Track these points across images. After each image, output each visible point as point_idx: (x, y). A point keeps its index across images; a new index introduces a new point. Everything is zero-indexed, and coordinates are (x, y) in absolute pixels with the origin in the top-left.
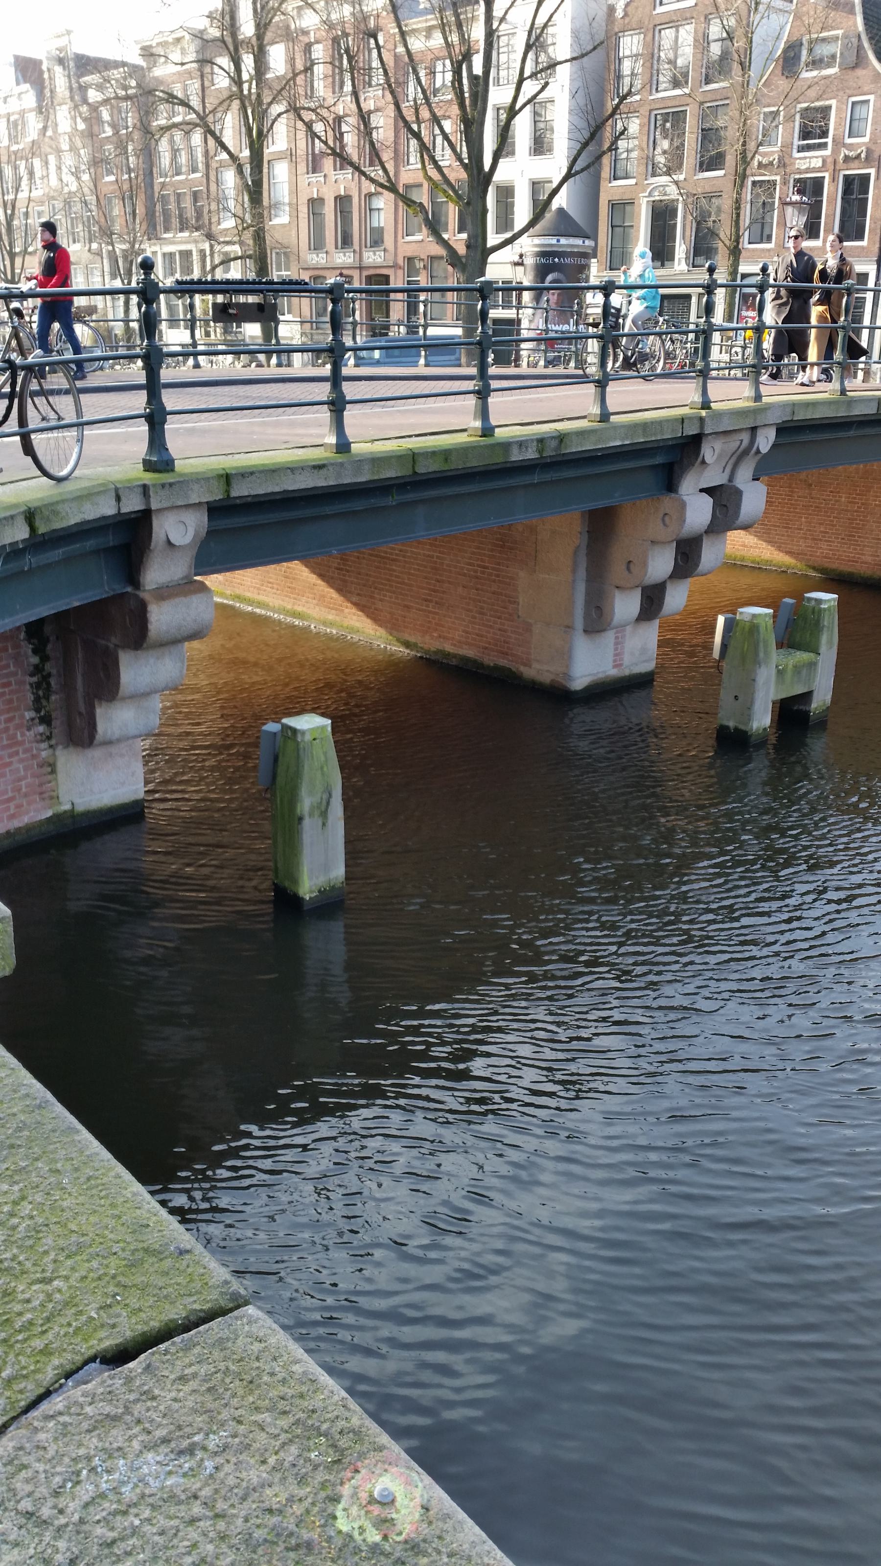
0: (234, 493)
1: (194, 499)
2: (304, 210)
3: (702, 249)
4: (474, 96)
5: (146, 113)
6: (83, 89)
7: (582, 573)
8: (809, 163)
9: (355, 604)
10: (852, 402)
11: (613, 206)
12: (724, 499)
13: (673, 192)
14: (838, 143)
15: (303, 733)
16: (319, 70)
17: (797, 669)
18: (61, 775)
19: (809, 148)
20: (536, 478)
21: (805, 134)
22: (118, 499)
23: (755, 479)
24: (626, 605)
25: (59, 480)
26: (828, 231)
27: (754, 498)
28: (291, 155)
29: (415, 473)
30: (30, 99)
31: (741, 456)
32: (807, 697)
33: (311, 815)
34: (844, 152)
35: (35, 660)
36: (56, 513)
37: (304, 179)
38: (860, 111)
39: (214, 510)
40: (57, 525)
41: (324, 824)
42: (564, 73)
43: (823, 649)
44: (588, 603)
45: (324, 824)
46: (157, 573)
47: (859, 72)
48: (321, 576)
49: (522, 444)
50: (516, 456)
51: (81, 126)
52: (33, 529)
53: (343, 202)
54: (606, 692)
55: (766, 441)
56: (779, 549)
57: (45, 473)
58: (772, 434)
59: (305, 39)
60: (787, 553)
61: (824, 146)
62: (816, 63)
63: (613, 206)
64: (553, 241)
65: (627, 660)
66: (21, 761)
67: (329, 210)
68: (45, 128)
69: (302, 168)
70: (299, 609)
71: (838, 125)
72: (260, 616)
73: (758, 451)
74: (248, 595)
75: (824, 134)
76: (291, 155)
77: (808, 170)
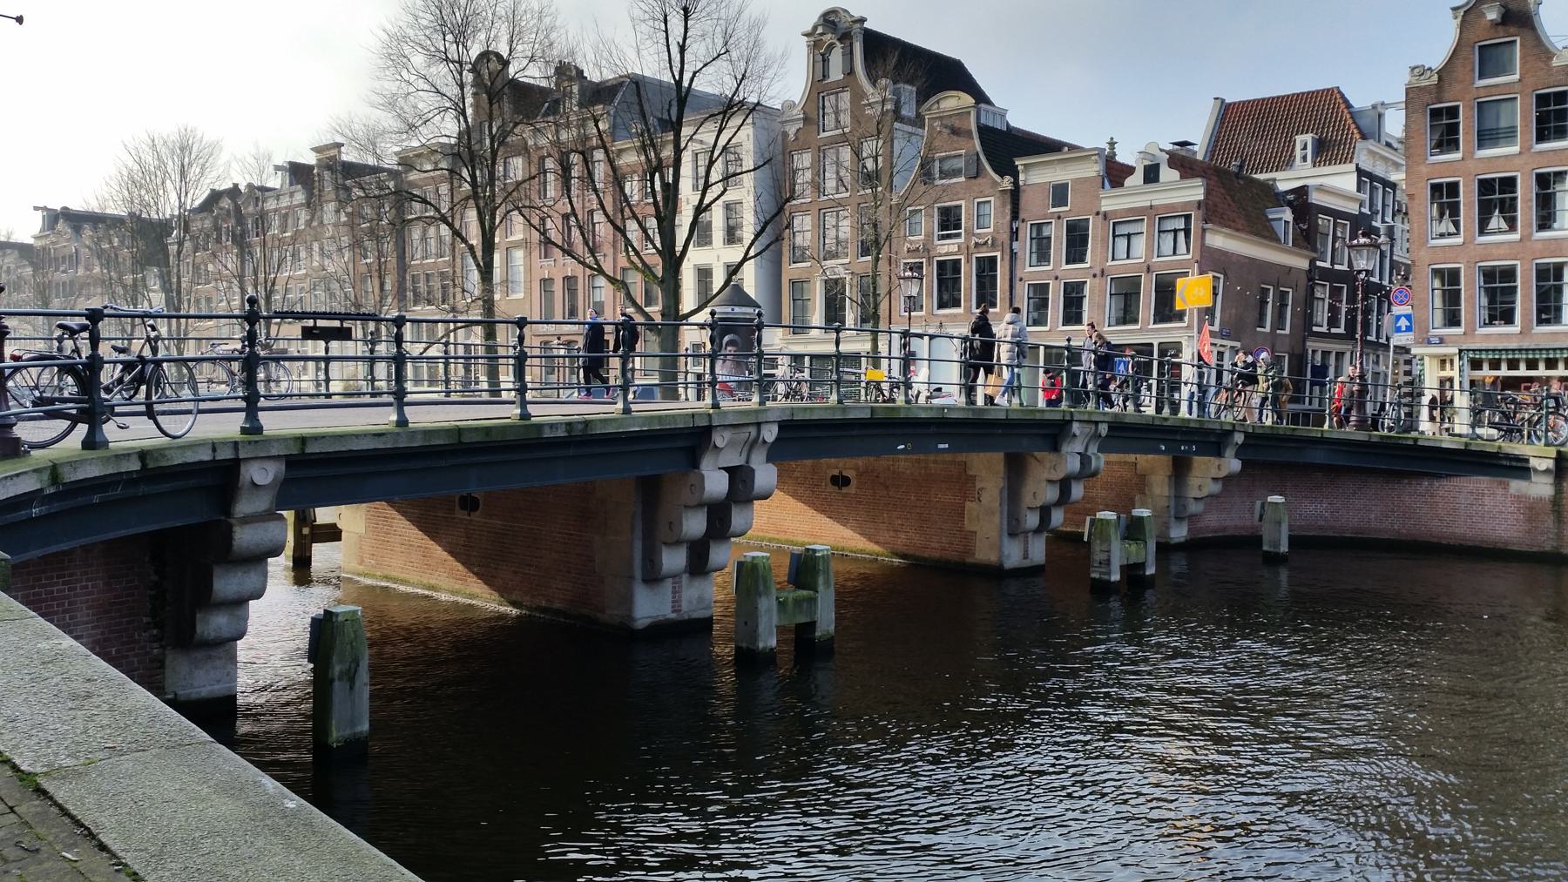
0: (308, 450)
1: (274, 452)
2: (536, 286)
3: (870, 317)
4: (666, 199)
5: (399, 207)
6: (348, 189)
7: (639, 533)
8: (948, 249)
9: (476, 574)
10: (845, 410)
11: (793, 283)
12: (740, 477)
13: (842, 273)
14: (969, 233)
15: (337, 615)
16: (551, 177)
17: (798, 602)
18: (168, 672)
19: (949, 237)
20: (571, 452)
21: (943, 227)
22: (214, 450)
23: (768, 461)
24: (674, 559)
25: (174, 437)
26: (969, 300)
27: (765, 474)
28: (525, 244)
29: (460, 443)
30: (300, 197)
31: (753, 444)
32: (812, 625)
33: (340, 679)
34: (975, 240)
35: (155, 578)
36: (164, 456)
37: (537, 261)
38: (985, 209)
39: (291, 462)
40: (164, 464)
41: (351, 688)
42: (748, 180)
43: (821, 588)
44: (644, 559)
45: (351, 688)
46: (245, 506)
47: (979, 180)
48: (451, 553)
49: (552, 426)
50: (547, 434)
51: (344, 219)
52: (144, 465)
53: (570, 281)
54: (663, 631)
55: (770, 434)
56: (870, 540)
57: (167, 435)
58: (775, 429)
59: (540, 153)
60: (877, 543)
61: (958, 235)
62: (945, 174)
63: (793, 283)
64: (729, 309)
65: (685, 606)
66: (136, 655)
67: (558, 287)
68: (311, 220)
69: (536, 254)
70: (433, 582)
71: (968, 219)
72: (408, 594)
73: (764, 442)
74: (394, 574)
75: (958, 226)
76: (525, 244)
77: (947, 254)
